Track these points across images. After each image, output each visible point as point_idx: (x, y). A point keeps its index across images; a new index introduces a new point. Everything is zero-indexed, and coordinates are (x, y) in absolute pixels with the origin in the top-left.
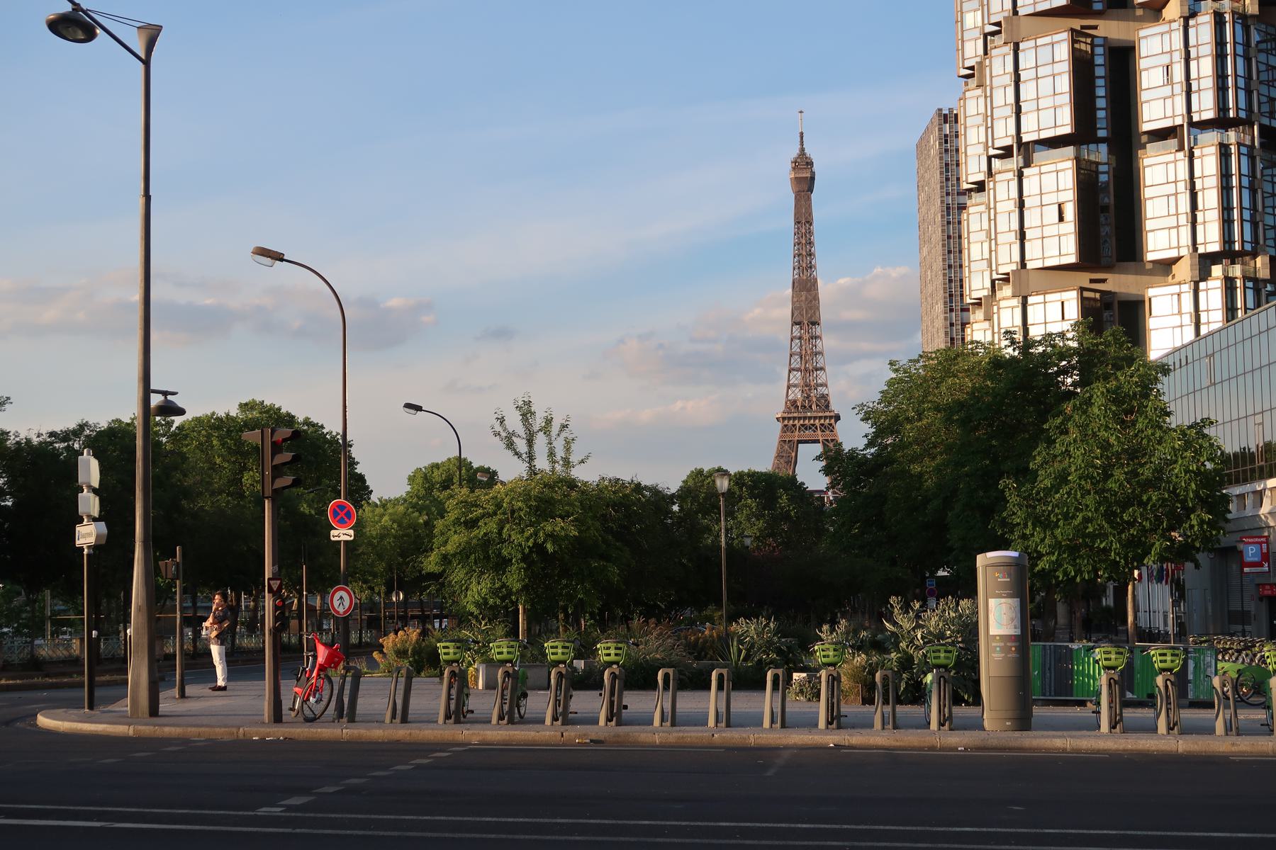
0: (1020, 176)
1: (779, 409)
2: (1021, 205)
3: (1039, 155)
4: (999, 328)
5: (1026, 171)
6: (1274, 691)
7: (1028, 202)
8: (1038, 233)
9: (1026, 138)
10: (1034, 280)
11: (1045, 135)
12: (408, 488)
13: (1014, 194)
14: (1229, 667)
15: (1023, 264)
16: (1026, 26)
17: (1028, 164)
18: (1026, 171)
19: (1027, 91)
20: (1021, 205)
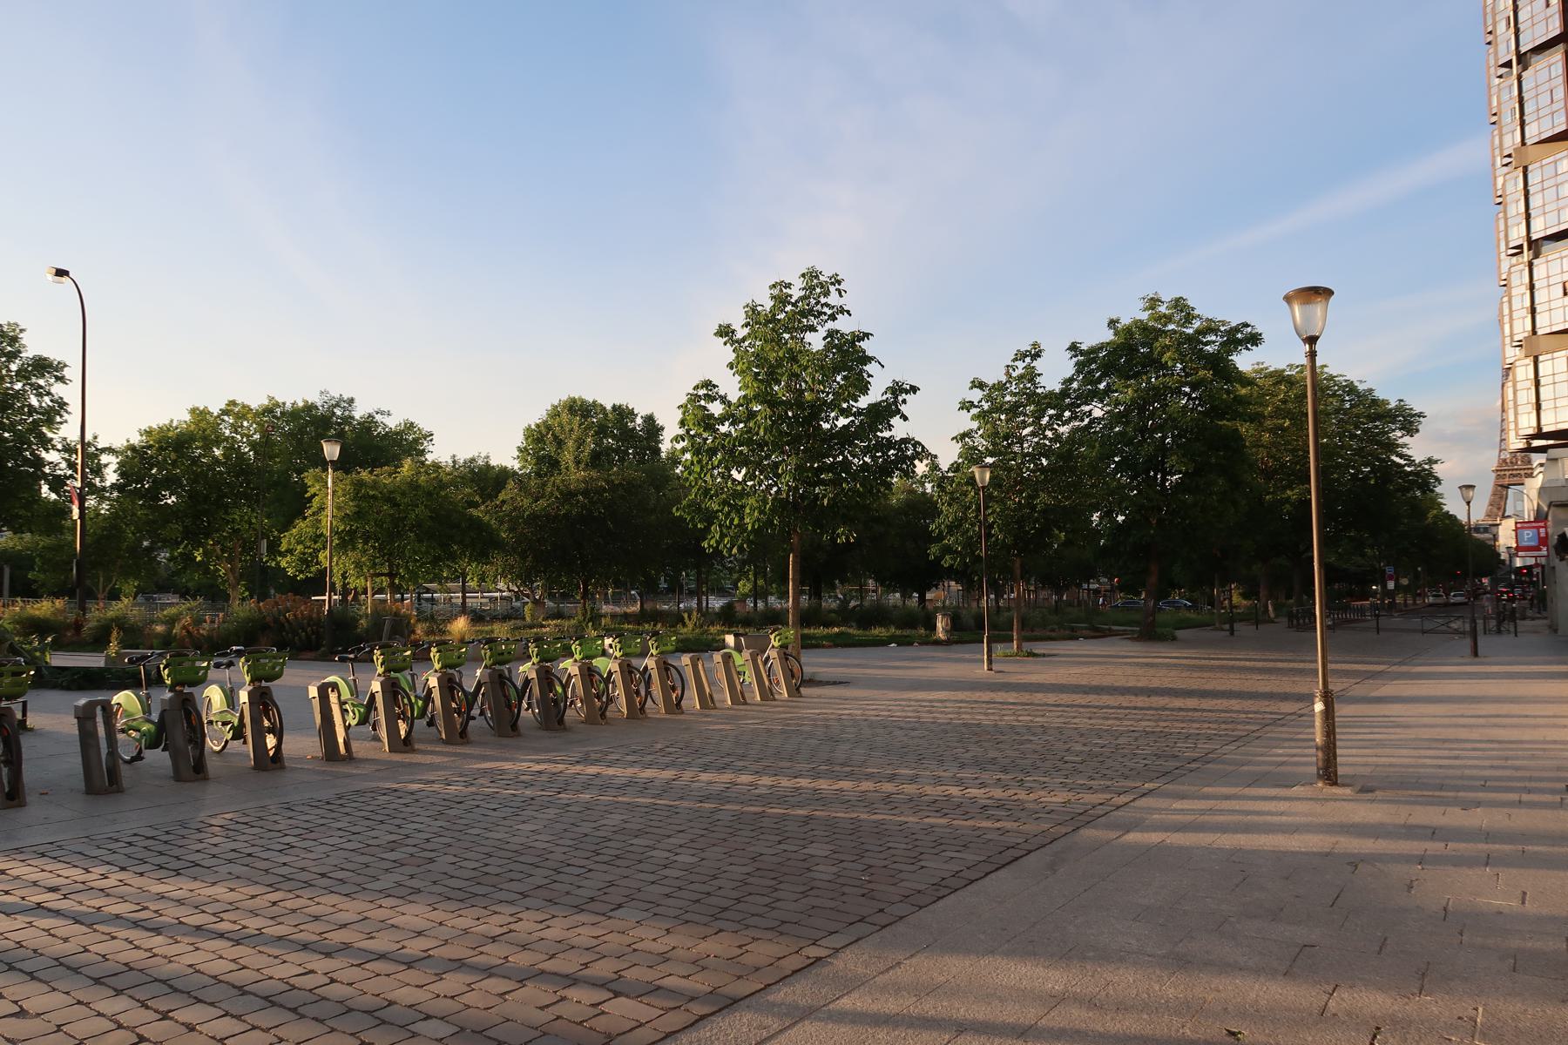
0: (1531, 265)
1: (1494, 465)
2: (1532, 287)
3: (1547, 248)
4: (1512, 335)
5: (1536, 262)
6: (158, 420)
7: (1539, 309)
8: (1550, 380)
9: (1534, 237)
10: (1544, 343)
11: (1549, 232)
12: (505, 453)
13: (1527, 280)
14: (45, 489)
15: (1534, 332)
16: (1532, 152)
17: (1537, 256)
18: (1536, 262)
19: (1535, 201)
20: (1532, 287)
